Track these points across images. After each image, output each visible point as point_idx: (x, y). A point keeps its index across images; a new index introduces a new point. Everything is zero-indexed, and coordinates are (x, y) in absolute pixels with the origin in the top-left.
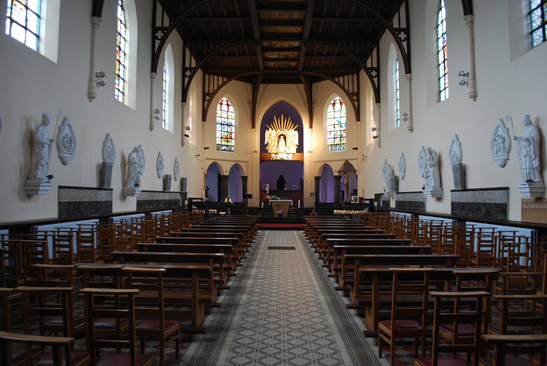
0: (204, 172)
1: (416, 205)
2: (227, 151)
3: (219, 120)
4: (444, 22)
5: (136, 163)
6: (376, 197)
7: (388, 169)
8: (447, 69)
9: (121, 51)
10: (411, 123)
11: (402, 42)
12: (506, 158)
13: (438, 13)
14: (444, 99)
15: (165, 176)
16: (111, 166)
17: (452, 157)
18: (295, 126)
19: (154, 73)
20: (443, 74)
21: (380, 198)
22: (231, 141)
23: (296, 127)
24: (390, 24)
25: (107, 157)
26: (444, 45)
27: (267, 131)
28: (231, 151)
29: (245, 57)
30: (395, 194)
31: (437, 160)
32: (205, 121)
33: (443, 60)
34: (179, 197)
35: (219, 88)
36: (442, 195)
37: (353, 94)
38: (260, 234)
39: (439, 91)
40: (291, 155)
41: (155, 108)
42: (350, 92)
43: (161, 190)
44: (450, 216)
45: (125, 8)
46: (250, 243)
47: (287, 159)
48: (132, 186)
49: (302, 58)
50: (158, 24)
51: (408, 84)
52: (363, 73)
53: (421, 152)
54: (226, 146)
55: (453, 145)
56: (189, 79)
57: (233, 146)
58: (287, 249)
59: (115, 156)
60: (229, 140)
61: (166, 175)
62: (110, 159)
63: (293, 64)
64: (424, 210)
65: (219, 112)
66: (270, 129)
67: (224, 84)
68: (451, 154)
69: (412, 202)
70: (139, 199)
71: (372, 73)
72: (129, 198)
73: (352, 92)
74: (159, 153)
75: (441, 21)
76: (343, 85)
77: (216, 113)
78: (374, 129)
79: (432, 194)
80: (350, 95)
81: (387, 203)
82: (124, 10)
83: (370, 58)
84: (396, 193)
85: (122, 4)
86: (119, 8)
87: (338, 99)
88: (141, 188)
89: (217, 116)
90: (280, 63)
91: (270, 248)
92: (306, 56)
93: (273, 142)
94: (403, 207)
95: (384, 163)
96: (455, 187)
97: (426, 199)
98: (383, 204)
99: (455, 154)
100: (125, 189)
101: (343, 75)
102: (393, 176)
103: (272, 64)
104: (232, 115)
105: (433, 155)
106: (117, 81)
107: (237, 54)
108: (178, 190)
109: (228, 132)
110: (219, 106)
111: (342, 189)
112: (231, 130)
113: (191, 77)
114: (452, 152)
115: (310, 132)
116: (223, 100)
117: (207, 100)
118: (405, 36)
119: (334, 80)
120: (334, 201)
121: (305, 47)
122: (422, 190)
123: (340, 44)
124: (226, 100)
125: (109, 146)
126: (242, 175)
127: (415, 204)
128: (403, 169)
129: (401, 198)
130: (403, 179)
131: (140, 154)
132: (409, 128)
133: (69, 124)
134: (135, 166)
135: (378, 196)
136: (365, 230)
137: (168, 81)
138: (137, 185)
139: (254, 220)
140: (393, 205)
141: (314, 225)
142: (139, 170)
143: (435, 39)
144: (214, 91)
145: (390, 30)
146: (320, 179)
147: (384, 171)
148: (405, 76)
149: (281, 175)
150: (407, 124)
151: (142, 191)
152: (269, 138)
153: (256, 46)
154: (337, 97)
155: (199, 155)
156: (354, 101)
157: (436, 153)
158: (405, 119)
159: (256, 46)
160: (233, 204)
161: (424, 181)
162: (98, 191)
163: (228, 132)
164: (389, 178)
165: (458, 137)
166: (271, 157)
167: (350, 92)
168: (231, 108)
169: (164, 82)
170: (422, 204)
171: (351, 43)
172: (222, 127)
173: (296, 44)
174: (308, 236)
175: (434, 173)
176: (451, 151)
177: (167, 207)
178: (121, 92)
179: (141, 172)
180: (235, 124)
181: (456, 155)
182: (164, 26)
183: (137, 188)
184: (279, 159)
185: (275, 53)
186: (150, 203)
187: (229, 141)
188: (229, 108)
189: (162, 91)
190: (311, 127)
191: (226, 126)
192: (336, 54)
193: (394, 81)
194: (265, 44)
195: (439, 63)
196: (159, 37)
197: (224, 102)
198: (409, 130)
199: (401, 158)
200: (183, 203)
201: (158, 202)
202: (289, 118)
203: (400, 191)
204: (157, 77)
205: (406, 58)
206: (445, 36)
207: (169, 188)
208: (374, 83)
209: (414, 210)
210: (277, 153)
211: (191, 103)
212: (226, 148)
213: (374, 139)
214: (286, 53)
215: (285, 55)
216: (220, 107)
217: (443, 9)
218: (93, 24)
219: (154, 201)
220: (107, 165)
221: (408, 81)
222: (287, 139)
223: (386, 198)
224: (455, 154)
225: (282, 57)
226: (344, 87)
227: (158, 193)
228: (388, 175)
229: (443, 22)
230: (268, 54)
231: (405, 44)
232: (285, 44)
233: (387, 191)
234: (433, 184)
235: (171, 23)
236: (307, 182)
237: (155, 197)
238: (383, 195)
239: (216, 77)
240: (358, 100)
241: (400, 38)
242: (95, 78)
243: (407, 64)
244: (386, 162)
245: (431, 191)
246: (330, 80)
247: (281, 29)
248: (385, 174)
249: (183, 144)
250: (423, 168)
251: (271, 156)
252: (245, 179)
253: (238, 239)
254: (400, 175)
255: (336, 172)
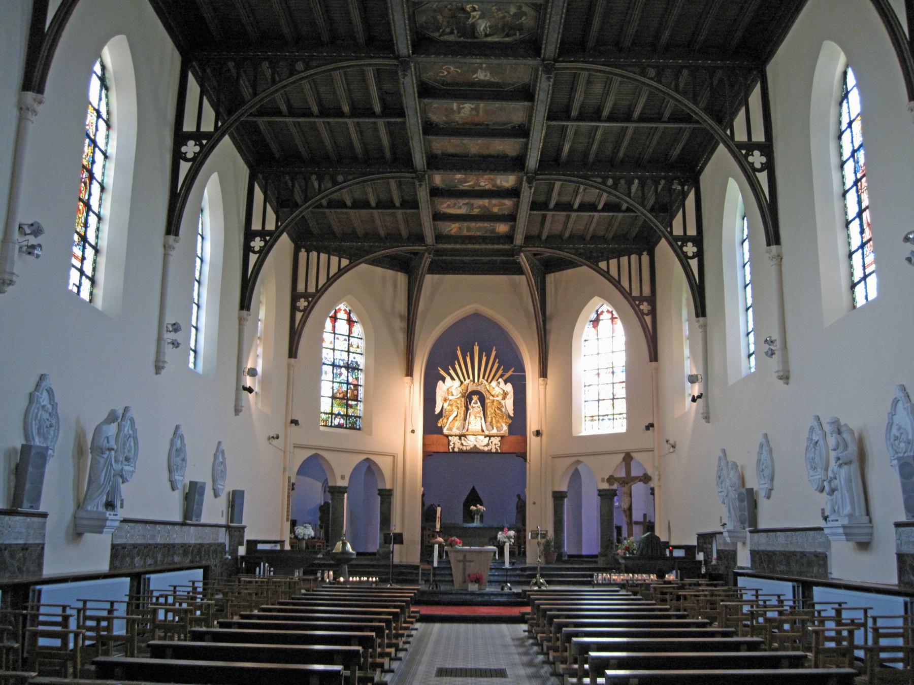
0: (289, 478)
1: (805, 560)
2: (346, 428)
3: (327, 355)
4: (857, 126)
5: (110, 449)
6: (702, 541)
7: (729, 475)
8: (867, 231)
9: (94, 182)
10: (785, 361)
11: (757, 173)
12: (823, 478)
13: (841, 104)
14: (864, 302)
15: (188, 483)
16: (43, 456)
17: (895, 440)
18: (506, 371)
19: (172, 238)
20: (859, 244)
21: (711, 543)
22: (357, 405)
23: (510, 373)
24: (728, 132)
25: (35, 431)
26: (859, 176)
27: (440, 382)
28: (355, 429)
29: (390, 211)
30: (748, 534)
31: (856, 448)
32: (296, 357)
33: (856, 210)
34: (223, 537)
35: (331, 281)
36: (871, 534)
37: (642, 299)
38: (420, 630)
39: (851, 284)
40: (496, 441)
41: (169, 320)
42: (634, 294)
43: (178, 518)
44: (897, 588)
45: (110, 82)
46: (382, 672)
47: (486, 449)
48: (97, 508)
49: (524, 213)
50: (256, 226)
51: (773, 270)
52: (663, 247)
53: (812, 429)
54: (342, 416)
55: (895, 410)
56: (258, 258)
57: (360, 417)
58: (486, 676)
59: (57, 430)
60: (350, 402)
61: (191, 482)
62: (45, 438)
63: (502, 228)
64: (826, 573)
65: (328, 337)
66: (448, 379)
67: (341, 272)
68: (890, 432)
69: (794, 553)
70: (118, 541)
71: (685, 249)
72: (88, 536)
73: (638, 294)
74: (177, 427)
75: (848, 121)
76: (617, 278)
77: (322, 340)
78: (693, 379)
79: (846, 534)
80: (676, 242)
81: (729, 556)
82: (107, 89)
83: (680, 214)
84: (751, 532)
85: (103, 74)
86: (95, 83)
87: (605, 310)
88: (122, 513)
89: (324, 345)
90: (473, 225)
91: (442, 672)
92: (532, 209)
93: (455, 409)
94: (771, 566)
95: (720, 459)
96: (907, 516)
97: (828, 544)
98: (719, 558)
99: (901, 434)
100: (81, 514)
101: (618, 255)
102: (744, 491)
103: (453, 228)
104: (359, 344)
105: (846, 436)
106: (77, 251)
107: (373, 204)
108: (223, 521)
109: (348, 383)
110: (328, 324)
111: (616, 522)
112: (357, 379)
113: (264, 253)
114: (894, 429)
115: (542, 387)
116: (340, 310)
117: (302, 308)
118: (764, 160)
119: (597, 265)
120: (599, 550)
121: (548, 79)
122: (821, 523)
123: (610, 182)
124: (345, 310)
125: (43, 407)
126: (380, 487)
127: (801, 558)
128: (767, 473)
129: (763, 543)
130: (768, 498)
131: (127, 430)
132: (781, 374)
133: (50, 388)
134: (109, 457)
135: (706, 539)
136: (738, 650)
137: (207, 257)
138: (110, 505)
139: (408, 597)
140: (744, 560)
141: (550, 610)
142: (117, 467)
143: (834, 161)
144: (319, 287)
145: (667, 239)
146: (566, 497)
147: (720, 477)
148: (767, 252)
149: (473, 490)
150: (774, 363)
151: (125, 521)
152: (445, 400)
153: (417, 183)
154: (605, 305)
155: (278, 438)
156: (643, 314)
157: (852, 432)
158: (770, 353)
159: (417, 183)
160: (354, 557)
161: (823, 500)
162: (7, 518)
163: (348, 383)
164: (734, 495)
165: (908, 390)
166: (449, 445)
167: (634, 294)
168: (358, 329)
169: (198, 261)
170: (822, 559)
171: (636, 181)
172: (335, 371)
173: (508, 181)
174: (548, 654)
175: (849, 481)
176: (890, 425)
177: (192, 562)
178: (87, 277)
179: (124, 473)
180: (366, 365)
181: (903, 437)
182: (267, 228)
183: (112, 513)
184: (468, 448)
185: (462, 202)
186: (146, 550)
187: (351, 406)
188: (354, 329)
189: (190, 280)
190: (543, 374)
191: (344, 370)
192: (600, 207)
193: (739, 264)
194: (438, 179)
195: (847, 220)
196: (190, 155)
197: (342, 315)
198: (781, 378)
199: (761, 446)
200: (234, 551)
201: (170, 548)
202: (494, 354)
203: (762, 525)
204: (179, 245)
205: (766, 209)
206: (861, 155)
207: (199, 515)
208: (693, 273)
209: (800, 574)
210: (465, 436)
211: (262, 314)
212: (342, 421)
213: (694, 404)
214: (485, 202)
215: (485, 206)
216: (331, 325)
217: (854, 97)
218: (21, 108)
219: (156, 546)
220: (198, 486)
221: (774, 262)
222: (487, 401)
223: (725, 543)
224: (901, 434)
225: (476, 211)
226: (619, 282)
227: (169, 527)
228: (730, 488)
229: (853, 125)
230: (445, 205)
231: (648, 319)
232: (485, 182)
233: (730, 527)
234: (848, 509)
235: (220, 124)
236: (534, 503)
237: (161, 537)
238: (718, 536)
239: (324, 257)
240: (653, 312)
241: (753, 164)
242: (16, 235)
243: (770, 223)
244: (725, 455)
245: (844, 527)
246: (588, 266)
247: (474, 146)
248: (723, 485)
249: (237, 411)
250: (819, 470)
251: (449, 442)
252: (386, 495)
253: (360, 648)
254: (762, 486)
255: (603, 480)
